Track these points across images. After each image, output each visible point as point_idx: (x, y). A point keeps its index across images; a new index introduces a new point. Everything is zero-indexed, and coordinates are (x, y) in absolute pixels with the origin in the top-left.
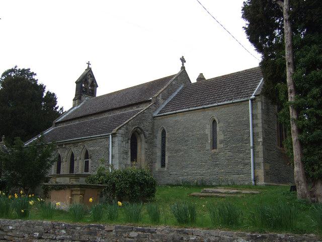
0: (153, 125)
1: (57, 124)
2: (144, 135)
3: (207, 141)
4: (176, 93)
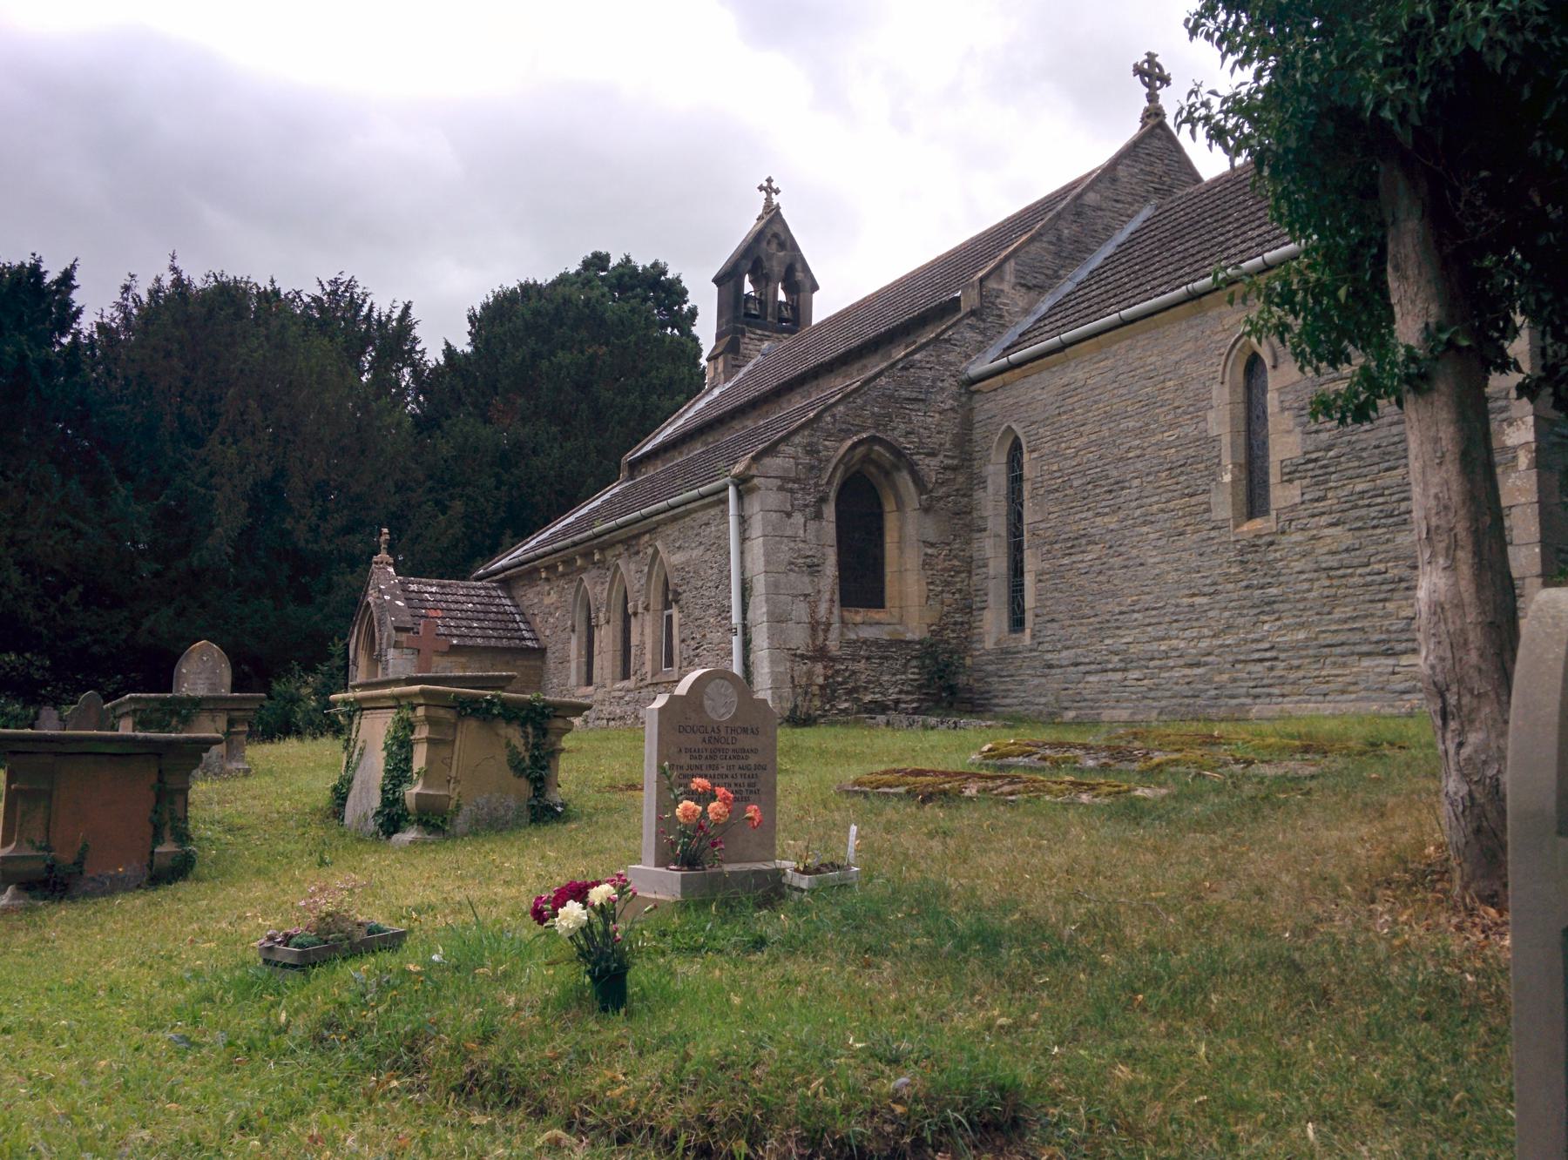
0: (967, 424)
1: (635, 466)
3: (1214, 476)
4: (1108, 249)
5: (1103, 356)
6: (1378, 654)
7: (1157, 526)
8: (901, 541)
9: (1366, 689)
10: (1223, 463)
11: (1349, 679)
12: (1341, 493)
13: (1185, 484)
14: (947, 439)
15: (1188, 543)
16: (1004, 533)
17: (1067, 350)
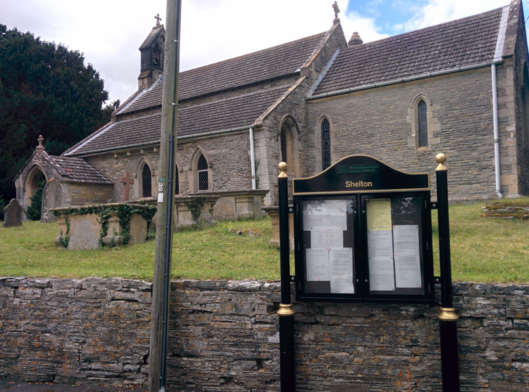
0: (307, 114)
2: (297, 128)
5: (365, 96)
6: (465, 184)
7: (387, 148)
8: (293, 149)
9: (461, 193)
10: (412, 130)
11: (456, 191)
12: (454, 141)
13: (398, 136)
14: (303, 117)
15: (398, 153)
16: (321, 148)
17: (350, 93)
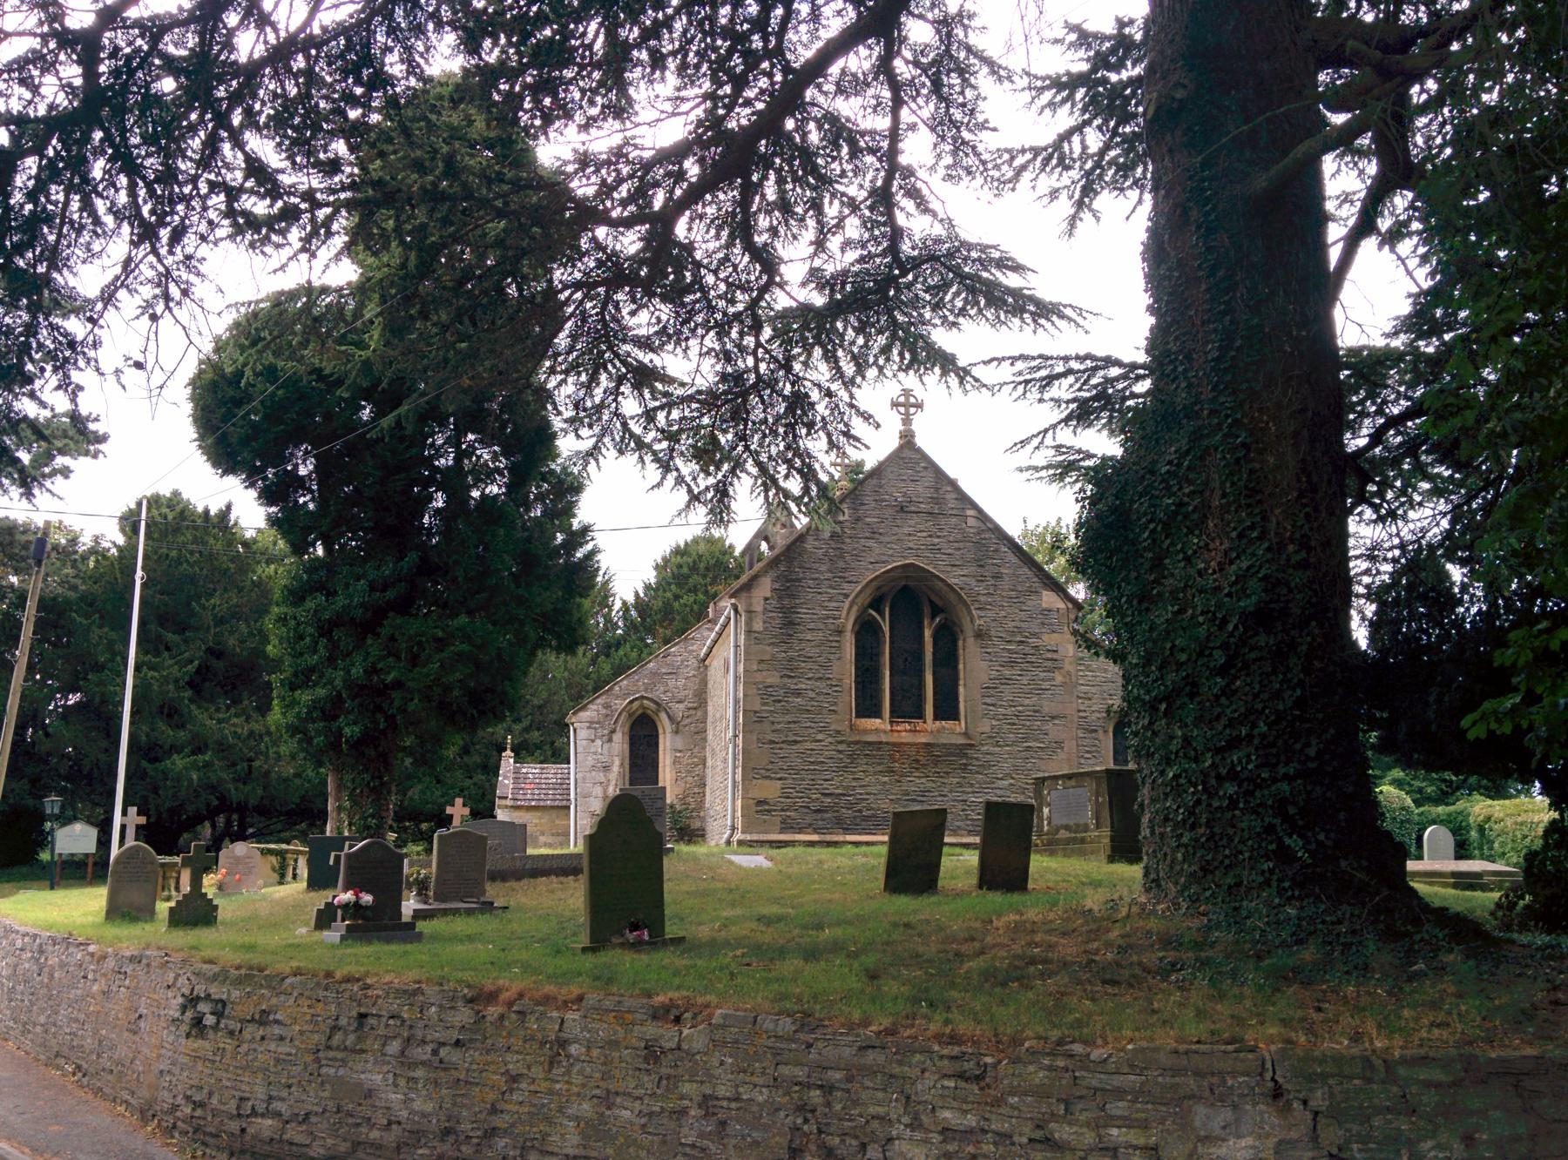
14: (690, 693)
